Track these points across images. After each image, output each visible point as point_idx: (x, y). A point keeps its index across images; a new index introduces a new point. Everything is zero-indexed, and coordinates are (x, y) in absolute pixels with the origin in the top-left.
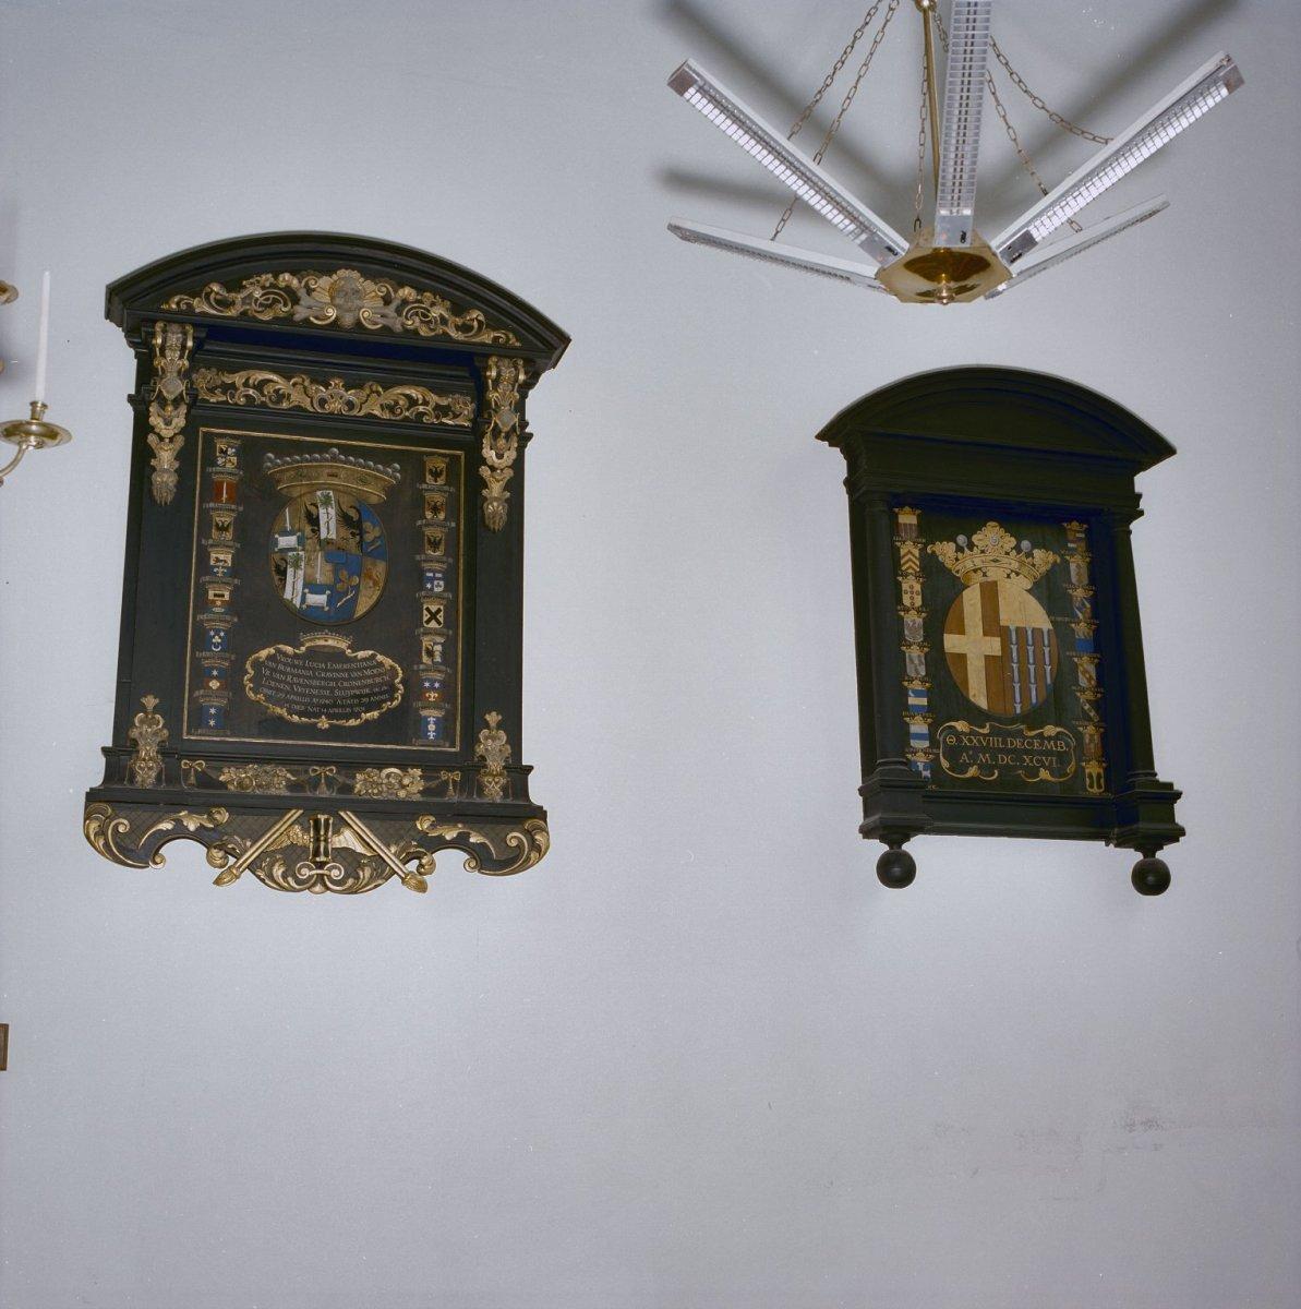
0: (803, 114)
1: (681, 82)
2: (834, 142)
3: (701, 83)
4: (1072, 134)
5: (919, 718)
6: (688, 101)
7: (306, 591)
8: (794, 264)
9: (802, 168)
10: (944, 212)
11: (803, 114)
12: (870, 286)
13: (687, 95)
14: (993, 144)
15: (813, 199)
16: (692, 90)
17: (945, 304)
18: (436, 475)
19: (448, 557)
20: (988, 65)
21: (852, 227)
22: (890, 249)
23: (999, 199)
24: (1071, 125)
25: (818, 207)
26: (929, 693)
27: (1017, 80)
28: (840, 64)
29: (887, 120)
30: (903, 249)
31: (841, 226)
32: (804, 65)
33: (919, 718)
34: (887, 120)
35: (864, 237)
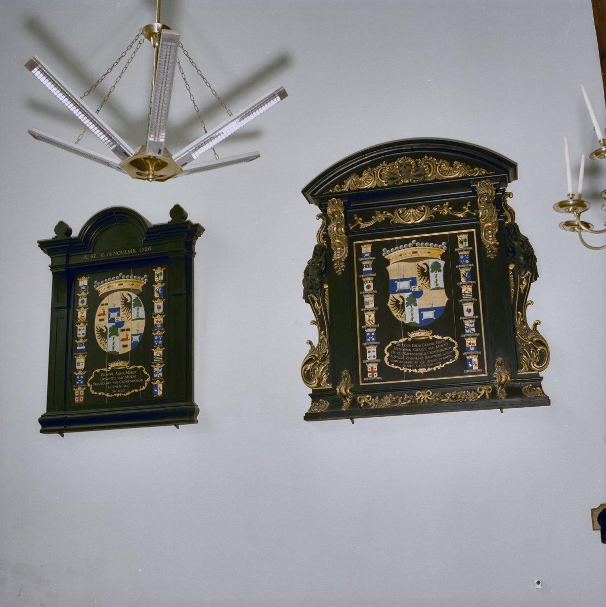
0: (92, 87)
1: (32, 65)
2: (106, 101)
3: (40, 66)
4: (219, 97)
5: (81, 356)
6: (34, 74)
7: (411, 280)
8: (69, 148)
9: (50, 76)
10: (151, 139)
11: (92, 87)
12: (118, 168)
13: (33, 72)
14: (180, 108)
15: (81, 117)
16: (36, 69)
17: (150, 181)
18: (469, 311)
19: (143, 276)
20: (178, 55)
21: (109, 141)
22: (125, 153)
23: (179, 135)
24: (221, 103)
25: (83, 120)
26: (86, 344)
27: (193, 64)
28: (115, 65)
29: (134, 96)
30: (132, 154)
31: (101, 138)
32: (96, 66)
33: (81, 356)
34: (134, 96)
35: (114, 146)
